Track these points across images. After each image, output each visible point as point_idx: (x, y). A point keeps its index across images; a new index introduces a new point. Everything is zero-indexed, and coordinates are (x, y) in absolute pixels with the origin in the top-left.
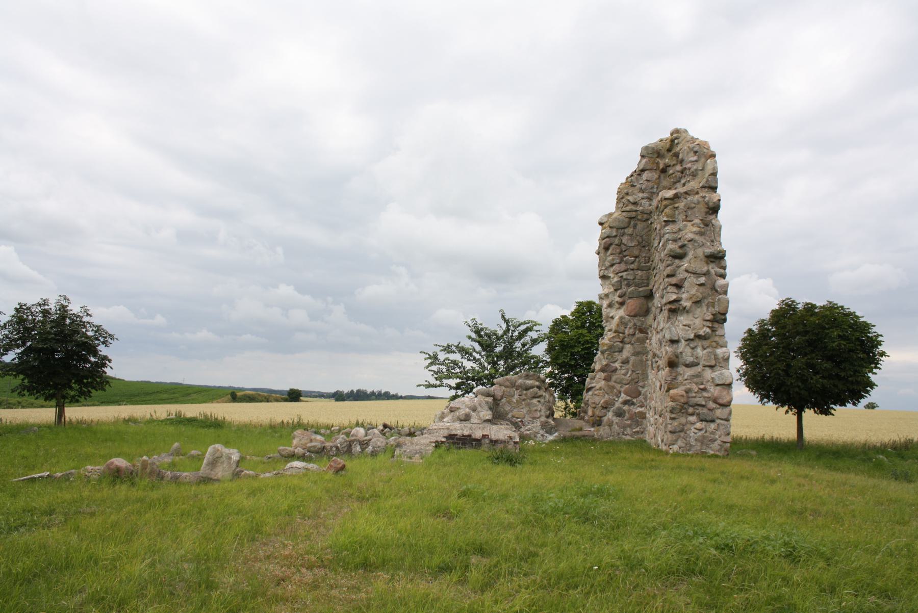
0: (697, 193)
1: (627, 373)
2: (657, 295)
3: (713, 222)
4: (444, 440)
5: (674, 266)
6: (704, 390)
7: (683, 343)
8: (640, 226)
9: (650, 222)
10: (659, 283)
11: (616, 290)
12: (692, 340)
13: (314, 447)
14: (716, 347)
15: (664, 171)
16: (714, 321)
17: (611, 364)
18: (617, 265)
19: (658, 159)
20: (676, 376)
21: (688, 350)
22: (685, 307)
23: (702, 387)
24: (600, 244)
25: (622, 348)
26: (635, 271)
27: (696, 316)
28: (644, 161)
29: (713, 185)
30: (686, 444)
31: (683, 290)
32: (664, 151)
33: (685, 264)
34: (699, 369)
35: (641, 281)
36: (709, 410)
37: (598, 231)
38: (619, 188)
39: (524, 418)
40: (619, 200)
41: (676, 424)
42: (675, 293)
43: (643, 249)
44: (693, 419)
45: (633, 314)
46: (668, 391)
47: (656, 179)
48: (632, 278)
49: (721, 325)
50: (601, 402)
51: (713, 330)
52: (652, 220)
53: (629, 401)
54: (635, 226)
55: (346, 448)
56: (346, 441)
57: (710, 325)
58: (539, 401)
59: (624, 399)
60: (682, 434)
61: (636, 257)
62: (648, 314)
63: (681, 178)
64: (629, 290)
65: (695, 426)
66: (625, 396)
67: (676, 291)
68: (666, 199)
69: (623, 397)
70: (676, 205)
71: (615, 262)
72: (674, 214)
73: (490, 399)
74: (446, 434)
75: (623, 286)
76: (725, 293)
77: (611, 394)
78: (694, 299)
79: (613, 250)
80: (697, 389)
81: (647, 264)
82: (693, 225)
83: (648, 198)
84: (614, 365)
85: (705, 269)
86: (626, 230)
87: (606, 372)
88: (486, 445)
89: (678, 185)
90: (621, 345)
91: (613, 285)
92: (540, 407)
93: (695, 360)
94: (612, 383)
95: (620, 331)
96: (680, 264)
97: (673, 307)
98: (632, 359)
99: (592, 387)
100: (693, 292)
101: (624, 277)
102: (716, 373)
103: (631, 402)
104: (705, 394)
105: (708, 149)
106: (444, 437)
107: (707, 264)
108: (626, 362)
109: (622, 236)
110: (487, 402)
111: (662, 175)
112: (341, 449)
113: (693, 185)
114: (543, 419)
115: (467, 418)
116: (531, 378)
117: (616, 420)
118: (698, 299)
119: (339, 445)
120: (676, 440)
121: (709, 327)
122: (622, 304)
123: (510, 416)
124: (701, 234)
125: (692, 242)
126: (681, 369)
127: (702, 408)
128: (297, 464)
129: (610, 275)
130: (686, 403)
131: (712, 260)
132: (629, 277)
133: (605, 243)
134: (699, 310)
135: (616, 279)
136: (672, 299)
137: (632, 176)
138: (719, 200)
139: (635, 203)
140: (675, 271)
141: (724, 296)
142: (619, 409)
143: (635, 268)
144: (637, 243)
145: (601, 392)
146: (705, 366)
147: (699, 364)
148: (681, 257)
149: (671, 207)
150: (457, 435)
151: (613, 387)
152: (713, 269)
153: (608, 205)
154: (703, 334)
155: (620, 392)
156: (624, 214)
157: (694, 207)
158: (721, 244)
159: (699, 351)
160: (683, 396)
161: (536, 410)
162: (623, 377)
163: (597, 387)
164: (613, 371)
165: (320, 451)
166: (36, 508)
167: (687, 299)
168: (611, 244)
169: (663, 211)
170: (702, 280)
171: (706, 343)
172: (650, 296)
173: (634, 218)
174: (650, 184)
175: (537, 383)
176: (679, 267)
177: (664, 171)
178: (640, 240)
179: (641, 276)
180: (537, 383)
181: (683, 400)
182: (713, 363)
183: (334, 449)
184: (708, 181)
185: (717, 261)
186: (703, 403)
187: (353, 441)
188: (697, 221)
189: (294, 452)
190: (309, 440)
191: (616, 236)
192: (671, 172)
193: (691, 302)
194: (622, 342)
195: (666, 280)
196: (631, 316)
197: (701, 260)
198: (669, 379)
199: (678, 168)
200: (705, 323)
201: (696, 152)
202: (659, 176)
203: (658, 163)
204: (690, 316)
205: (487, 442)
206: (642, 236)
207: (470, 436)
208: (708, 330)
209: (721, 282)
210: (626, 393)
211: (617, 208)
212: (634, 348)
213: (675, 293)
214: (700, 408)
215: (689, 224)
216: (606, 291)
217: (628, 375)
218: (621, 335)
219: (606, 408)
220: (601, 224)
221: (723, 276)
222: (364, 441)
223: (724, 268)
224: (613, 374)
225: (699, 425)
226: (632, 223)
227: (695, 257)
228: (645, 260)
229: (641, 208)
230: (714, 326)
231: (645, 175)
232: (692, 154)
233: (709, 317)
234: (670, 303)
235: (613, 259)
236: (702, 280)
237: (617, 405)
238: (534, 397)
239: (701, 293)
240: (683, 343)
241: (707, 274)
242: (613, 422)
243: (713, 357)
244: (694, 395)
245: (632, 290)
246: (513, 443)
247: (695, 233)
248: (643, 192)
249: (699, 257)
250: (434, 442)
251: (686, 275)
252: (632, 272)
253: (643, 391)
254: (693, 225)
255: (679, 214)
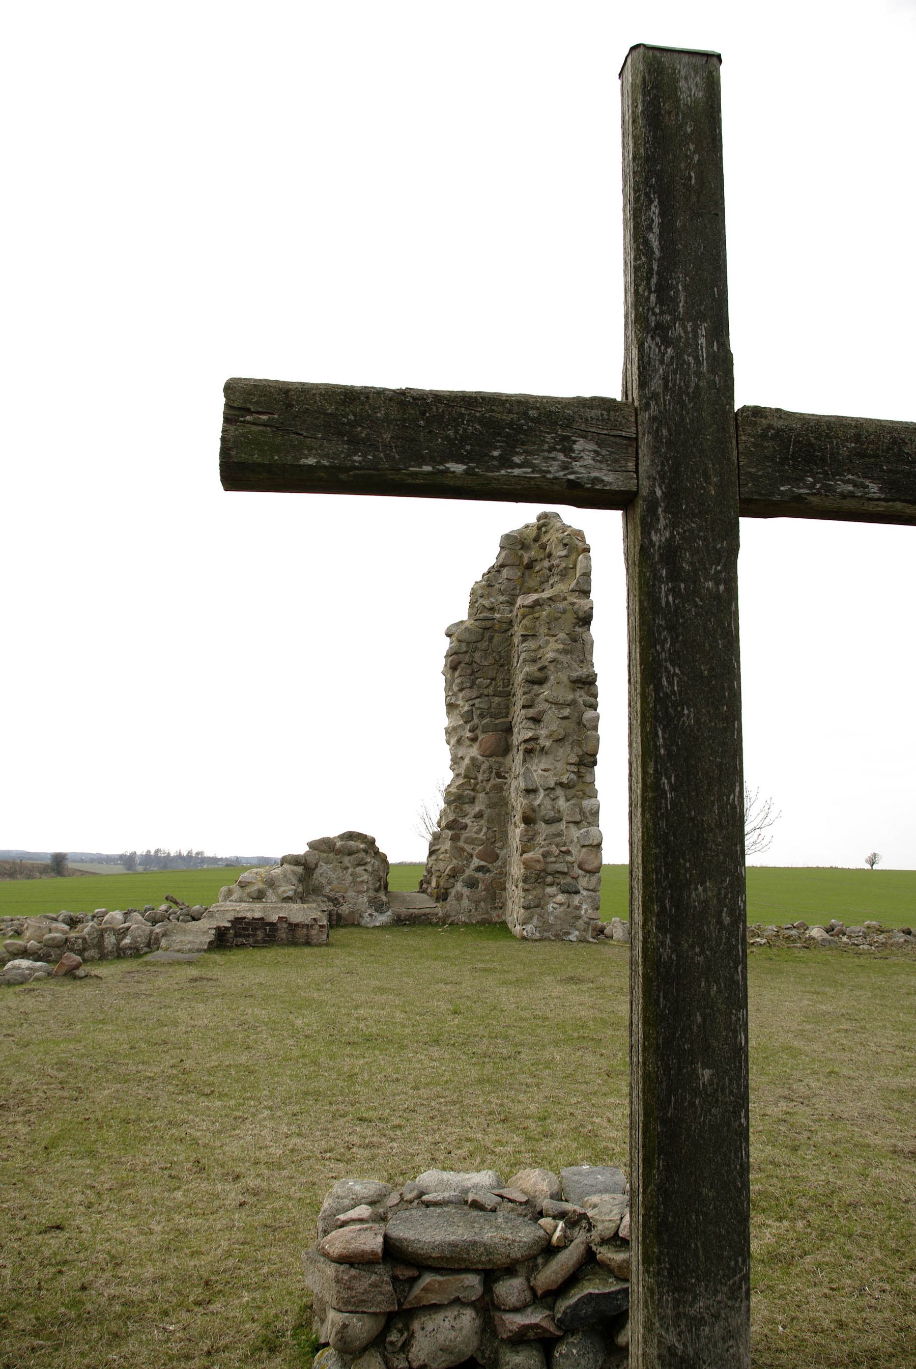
0: (565, 599)
1: (481, 830)
2: (516, 730)
3: (584, 636)
4: (229, 925)
5: (532, 694)
6: (568, 853)
7: (542, 793)
8: (497, 638)
9: (510, 634)
10: (519, 715)
11: (466, 722)
12: (553, 789)
13: (53, 939)
14: (582, 798)
15: (530, 566)
16: (580, 764)
17: (460, 819)
18: (468, 690)
19: (521, 552)
20: (534, 835)
21: (548, 803)
22: (544, 747)
23: (564, 849)
24: (446, 662)
25: (474, 798)
26: (491, 698)
27: (558, 759)
28: (504, 554)
29: (585, 588)
30: (544, 923)
31: (542, 724)
32: (529, 541)
33: (546, 692)
34: (562, 826)
35: (497, 711)
36: (573, 878)
37: (445, 644)
38: (472, 589)
39: (346, 892)
40: (472, 604)
41: (530, 897)
42: (531, 729)
43: (501, 669)
44: (550, 890)
45: (487, 753)
46: (521, 855)
47: (519, 578)
48: (486, 707)
49: (590, 769)
50: (448, 870)
51: (580, 776)
52: (512, 631)
53: (483, 867)
54: (491, 639)
55: (97, 939)
56: (97, 930)
57: (576, 770)
58: (366, 870)
59: (476, 865)
60: (538, 910)
61: (492, 679)
62: (507, 754)
63: (549, 577)
64: (483, 723)
65: (554, 900)
66: (478, 860)
67: (533, 727)
68: (523, 607)
69: (476, 862)
70: (537, 615)
71: (465, 686)
72: (535, 627)
73: (299, 869)
74: (231, 918)
75: (475, 717)
76: (595, 728)
77: (460, 859)
78: (555, 737)
79: (462, 670)
80: (558, 851)
81: (506, 689)
82: (556, 641)
83: (507, 602)
84: (464, 821)
85: (570, 697)
86: (479, 645)
87: (453, 829)
88: (283, 930)
89: (546, 586)
90: (472, 793)
91: (462, 716)
92: (365, 877)
93: (557, 815)
94: (461, 844)
95: (471, 776)
96: (539, 692)
97: (529, 747)
98: (487, 812)
99: (438, 850)
100: (554, 727)
101: (477, 706)
102: (582, 831)
103: (485, 869)
104: (569, 858)
105: (583, 539)
106: (229, 921)
107: (574, 690)
108: (479, 816)
109: (474, 652)
110: (294, 873)
111: (527, 573)
112: (89, 941)
113: (561, 588)
114: (372, 894)
115: (259, 896)
116: (355, 839)
117: (466, 891)
118: (560, 737)
119: (87, 936)
120: (531, 918)
121: (574, 772)
122: (474, 740)
123: (327, 889)
124: (565, 652)
125: (554, 664)
126: (541, 826)
127: (563, 876)
128: (25, 963)
129: (458, 703)
130: (544, 870)
131: (580, 686)
132: (482, 706)
133: (451, 661)
134: (561, 750)
135: (466, 708)
136: (527, 737)
137: (489, 572)
138: (592, 608)
139: (492, 609)
140: (533, 700)
141: (594, 733)
142: (470, 877)
143: (491, 693)
144: (493, 662)
145: (448, 855)
146: (568, 822)
147: (561, 820)
148: (541, 682)
149: (531, 616)
150: (245, 918)
151: (463, 850)
152: (581, 697)
153: (460, 612)
154: (566, 782)
155: (472, 856)
156: (477, 623)
157: (560, 618)
158: (592, 665)
159: (562, 803)
160: (539, 861)
161: (362, 882)
162: (476, 836)
163: (442, 850)
164: (462, 829)
165: (61, 944)
166: (840, 1138)
167: (546, 737)
168: (460, 663)
169: (521, 622)
170: (566, 712)
171: (571, 792)
172: (509, 730)
173: (489, 628)
174: (512, 584)
175: (362, 846)
176: (538, 695)
177: (530, 566)
178: (497, 658)
179: (499, 704)
180: (362, 846)
181: (538, 867)
182: (578, 818)
183: (80, 941)
184: (578, 583)
185: (586, 688)
186: (566, 870)
187: (105, 930)
188: (562, 635)
189: (26, 947)
190: (47, 930)
191: (466, 652)
192: (537, 568)
193: (551, 741)
194: (473, 790)
195: (523, 712)
196: (486, 756)
197: (565, 686)
198: (525, 839)
199: (546, 564)
200: (568, 767)
201: (565, 545)
202: (523, 574)
203: (521, 557)
204: (551, 757)
205: (285, 926)
206: (499, 652)
207: (262, 919)
208: (573, 776)
209: (589, 714)
210: (480, 857)
211: (470, 615)
212: (490, 797)
213: (531, 729)
214: (561, 876)
215: (552, 639)
216: (455, 724)
217: (482, 834)
218: (472, 781)
219: (454, 877)
220: (449, 635)
221: (594, 707)
222: (120, 929)
223: (595, 696)
224: (463, 832)
225: (561, 898)
226: (487, 634)
227: (558, 683)
228: (503, 683)
229: (498, 616)
230: (581, 770)
231: (505, 572)
232: (561, 547)
233: (574, 759)
234: (525, 741)
235: (462, 683)
236: (566, 712)
237: (469, 872)
238: (359, 865)
239: (564, 729)
240: (542, 793)
241: (572, 704)
242: (462, 895)
243: (578, 810)
244: (553, 859)
245: (487, 723)
246: (317, 927)
247: (560, 652)
248: (503, 595)
249: (563, 682)
250: (215, 928)
251: (546, 706)
252: (487, 698)
253: (502, 853)
254: (556, 641)
255: (540, 625)
